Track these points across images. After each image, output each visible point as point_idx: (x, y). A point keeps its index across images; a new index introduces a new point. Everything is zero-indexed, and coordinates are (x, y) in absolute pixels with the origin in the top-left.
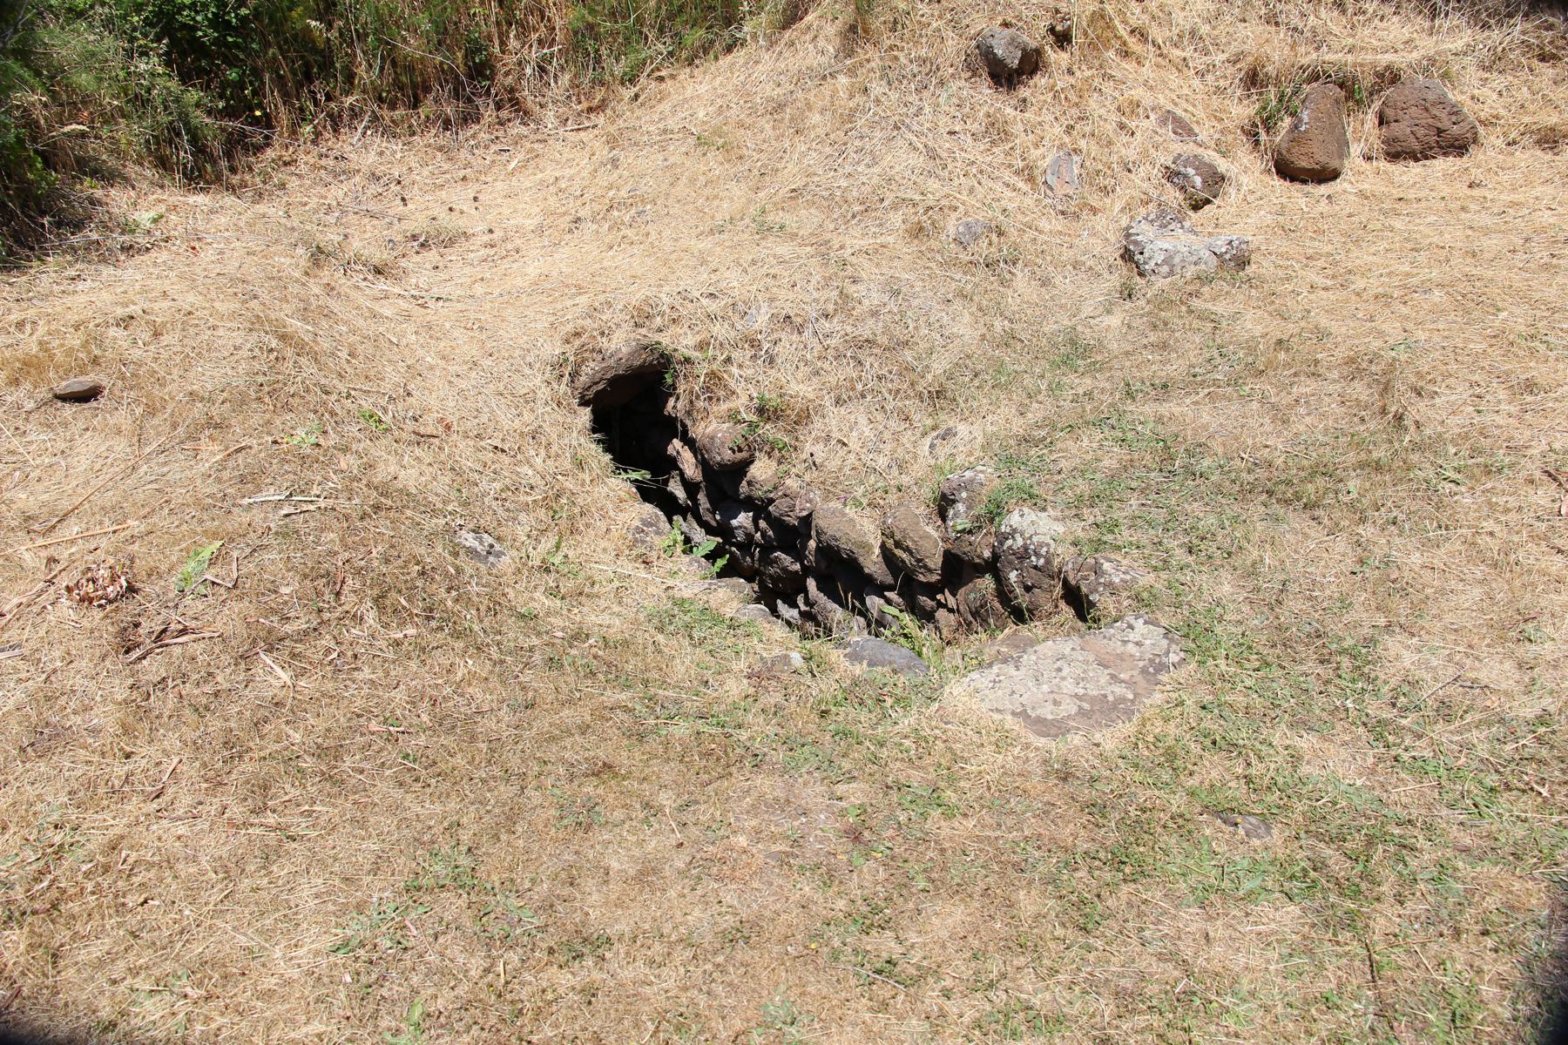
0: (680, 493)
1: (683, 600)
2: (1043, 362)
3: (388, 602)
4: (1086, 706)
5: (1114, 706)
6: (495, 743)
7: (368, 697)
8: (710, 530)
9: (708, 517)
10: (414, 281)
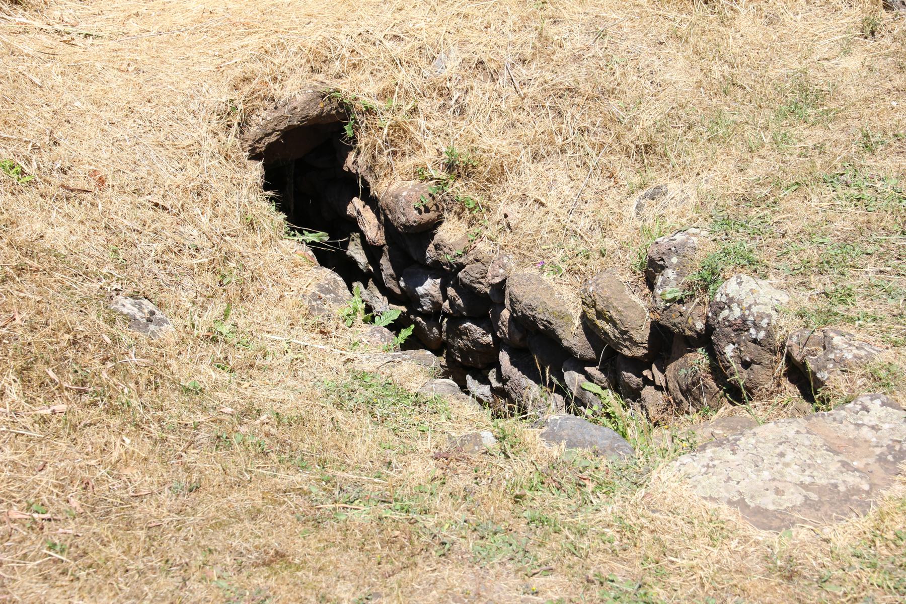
0: (361, 258)
1: (364, 374)
2: (767, 112)
3: (33, 375)
4: (814, 496)
5: (847, 498)
6: (154, 530)
7: (10, 481)
8: (393, 299)
9: (391, 284)
10: (57, 14)
